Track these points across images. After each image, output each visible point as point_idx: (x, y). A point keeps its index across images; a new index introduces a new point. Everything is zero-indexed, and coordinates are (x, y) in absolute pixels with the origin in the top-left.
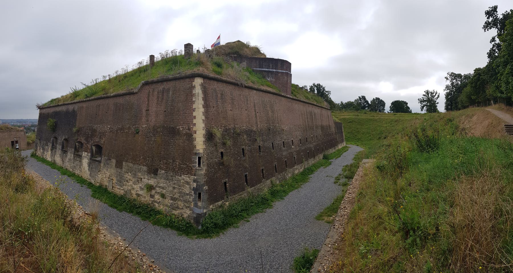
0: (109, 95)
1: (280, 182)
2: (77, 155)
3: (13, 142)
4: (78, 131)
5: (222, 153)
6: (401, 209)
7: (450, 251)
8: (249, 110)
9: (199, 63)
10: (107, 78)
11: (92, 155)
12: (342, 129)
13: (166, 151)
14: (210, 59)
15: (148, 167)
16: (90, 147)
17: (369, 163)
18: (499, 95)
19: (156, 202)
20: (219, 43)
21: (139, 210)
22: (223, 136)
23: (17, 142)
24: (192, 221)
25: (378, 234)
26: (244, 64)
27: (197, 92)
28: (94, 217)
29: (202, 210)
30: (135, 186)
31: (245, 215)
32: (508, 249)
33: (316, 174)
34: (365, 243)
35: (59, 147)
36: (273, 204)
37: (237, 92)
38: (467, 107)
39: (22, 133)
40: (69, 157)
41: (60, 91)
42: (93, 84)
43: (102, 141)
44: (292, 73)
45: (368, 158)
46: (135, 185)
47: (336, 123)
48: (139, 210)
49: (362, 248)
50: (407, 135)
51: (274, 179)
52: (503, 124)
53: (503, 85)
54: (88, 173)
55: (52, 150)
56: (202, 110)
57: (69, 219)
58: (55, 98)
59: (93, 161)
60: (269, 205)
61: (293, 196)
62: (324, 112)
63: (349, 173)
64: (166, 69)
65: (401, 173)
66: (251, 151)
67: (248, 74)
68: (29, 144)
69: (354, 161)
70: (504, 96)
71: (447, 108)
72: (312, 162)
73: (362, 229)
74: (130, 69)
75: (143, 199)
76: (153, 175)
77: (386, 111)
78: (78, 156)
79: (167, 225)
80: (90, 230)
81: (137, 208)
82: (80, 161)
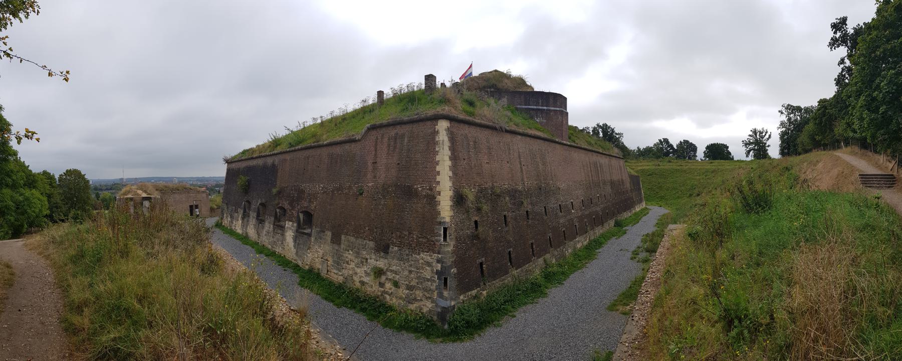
0: (321, 143)
1: (556, 260)
2: (278, 226)
3: (191, 207)
4: (279, 192)
5: (476, 222)
6: (721, 291)
7: (789, 347)
8: (512, 162)
9: (445, 100)
10: (319, 121)
11: (299, 226)
12: (639, 185)
13: (398, 219)
14: (459, 96)
15: (376, 242)
16: (295, 215)
17: (677, 230)
18: (851, 134)
19: (387, 293)
20: (471, 74)
21: (365, 305)
22: (478, 198)
23: (197, 207)
24: (435, 318)
25: (692, 326)
26: (505, 101)
27: (441, 139)
28: (303, 314)
29: (448, 302)
30: (358, 270)
31: (509, 307)
32: (864, 339)
33: (605, 247)
34: (675, 338)
35: (253, 215)
36: (547, 291)
37: (494, 138)
38: (810, 150)
39: (204, 195)
40: (266, 228)
41: (256, 136)
42: (299, 128)
43: (313, 206)
44: (568, 111)
45: (675, 223)
46: (359, 269)
47: (631, 177)
48: (365, 305)
49: (671, 347)
50: (729, 190)
51: (548, 256)
52: (857, 173)
53: (856, 122)
54: (293, 250)
55: (243, 219)
56: (448, 163)
57: (269, 317)
58: (247, 148)
59: (300, 233)
60: (542, 292)
61: (575, 280)
62: (614, 162)
63: (651, 245)
64: (399, 108)
65: (721, 241)
66: (515, 219)
67: (509, 114)
68: (212, 210)
69: (656, 228)
70: (858, 136)
71: (782, 153)
72: (599, 231)
73: (672, 321)
74: (350, 109)
75: (369, 289)
76: (382, 254)
77: (698, 158)
78: (279, 227)
79: (401, 326)
80: (297, 334)
81: (361, 302)
82: (283, 235)
